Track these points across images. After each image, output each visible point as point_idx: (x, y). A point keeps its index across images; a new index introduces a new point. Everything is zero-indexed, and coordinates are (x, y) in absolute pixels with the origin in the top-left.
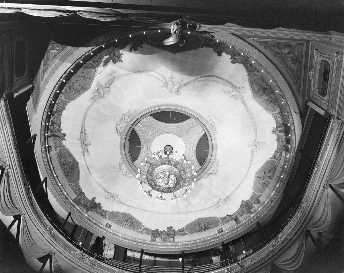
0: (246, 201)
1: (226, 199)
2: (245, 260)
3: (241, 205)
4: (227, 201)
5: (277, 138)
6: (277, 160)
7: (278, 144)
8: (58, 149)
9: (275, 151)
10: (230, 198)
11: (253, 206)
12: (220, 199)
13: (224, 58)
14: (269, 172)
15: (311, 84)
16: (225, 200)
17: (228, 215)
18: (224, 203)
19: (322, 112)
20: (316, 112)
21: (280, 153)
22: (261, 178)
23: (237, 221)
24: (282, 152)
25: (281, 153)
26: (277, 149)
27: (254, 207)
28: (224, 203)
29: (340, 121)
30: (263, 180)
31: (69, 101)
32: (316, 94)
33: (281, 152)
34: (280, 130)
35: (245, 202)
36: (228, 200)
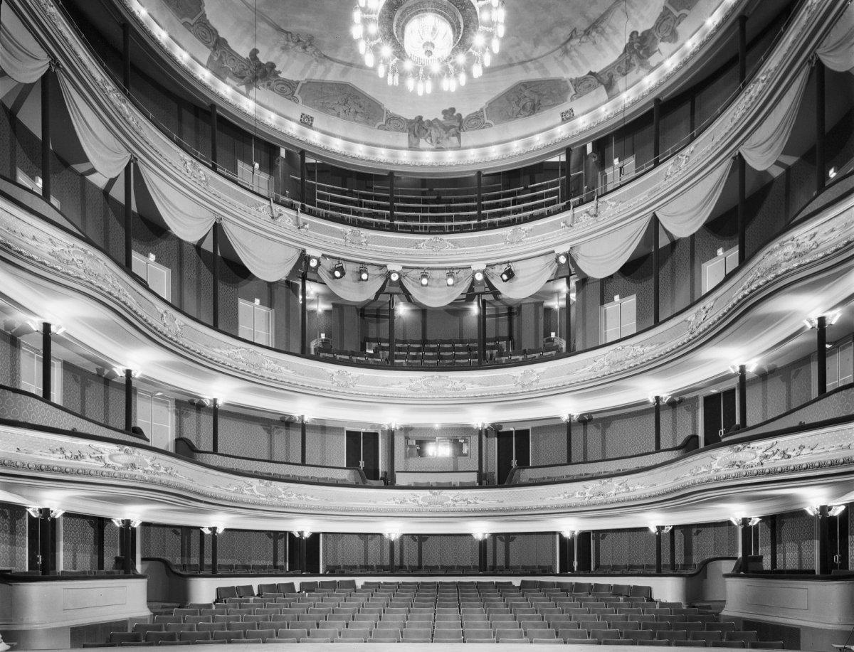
0: (643, 33)
35: (639, 35)
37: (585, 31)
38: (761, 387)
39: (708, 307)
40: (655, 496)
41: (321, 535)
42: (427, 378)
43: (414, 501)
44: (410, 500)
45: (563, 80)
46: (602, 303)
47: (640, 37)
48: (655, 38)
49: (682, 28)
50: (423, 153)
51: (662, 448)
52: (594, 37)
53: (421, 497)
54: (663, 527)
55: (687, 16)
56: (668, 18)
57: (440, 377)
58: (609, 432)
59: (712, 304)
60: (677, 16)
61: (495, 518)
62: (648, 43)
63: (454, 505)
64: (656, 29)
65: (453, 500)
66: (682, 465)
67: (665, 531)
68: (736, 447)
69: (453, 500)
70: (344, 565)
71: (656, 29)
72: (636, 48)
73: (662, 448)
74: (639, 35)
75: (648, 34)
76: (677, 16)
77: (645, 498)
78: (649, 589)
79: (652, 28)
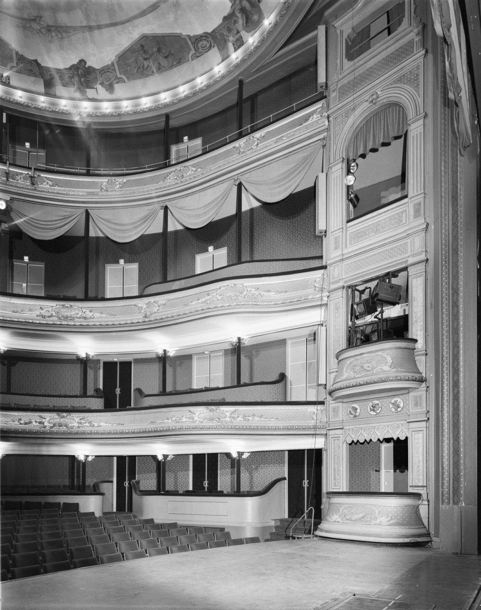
0: (90, 67)
1: (53, 29)
2: (42, 175)
3: (74, 65)
4: (53, 34)
5: (229, 15)
6: (195, 50)
7: (220, 25)
8: (119, 76)
9: (204, 33)
10: (64, 34)
11: (95, 87)
12: (41, 17)
13: (400, 584)
14: (166, 55)
15: (355, 6)
16: (49, 29)
17: (36, 61)
18: (43, 30)
19: (321, 79)
20: (316, 47)
21: (208, 45)
22: (145, 52)
23: (50, 88)
24: (214, 47)
25: (210, 46)
26: (212, 32)
27: (96, 89)
28: (43, 30)
29: (327, 123)
30: (145, 59)
31: (188, 40)
32: (344, 34)
33: (212, 45)
34: (245, 8)
35: (86, 66)
36: (56, 35)
37: (48, 26)
38: (158, 365)
39: (160, 303)
40: (149, 432)
41: (219, 455)
42: (58, 306)
43: (40, 423)
44: (36, 422)
45: (10, 47)
46: (11, 257)
47: (86, 68)
48: (97, 78)
49: (120, 90)
50: (103, 103)
51: (88, 394)
52: (52, 37)
53: (48, 419)
54: (167, 456)
55: (125, 82)
56: (112, 73)
57: (71, 306)
58: (14, 369)
59: (164, 302)
60: (118, 77)
61: (94, 441)
62: (91, 77)
63: (79, 427)
64: (100, 72)
65: (78, 423)
66: (154, 413)
67: (169, 459)
68: (210, 407)
69: (78, 423)
70: (63, 485)
71: (100, 72)
72: (80, 73)
73: (88, 394)
74: (86, 66)
75: (92, 71)
76: (118, 77)
77: (114, 434)
78: (77, 505)
79: (98, 69)
